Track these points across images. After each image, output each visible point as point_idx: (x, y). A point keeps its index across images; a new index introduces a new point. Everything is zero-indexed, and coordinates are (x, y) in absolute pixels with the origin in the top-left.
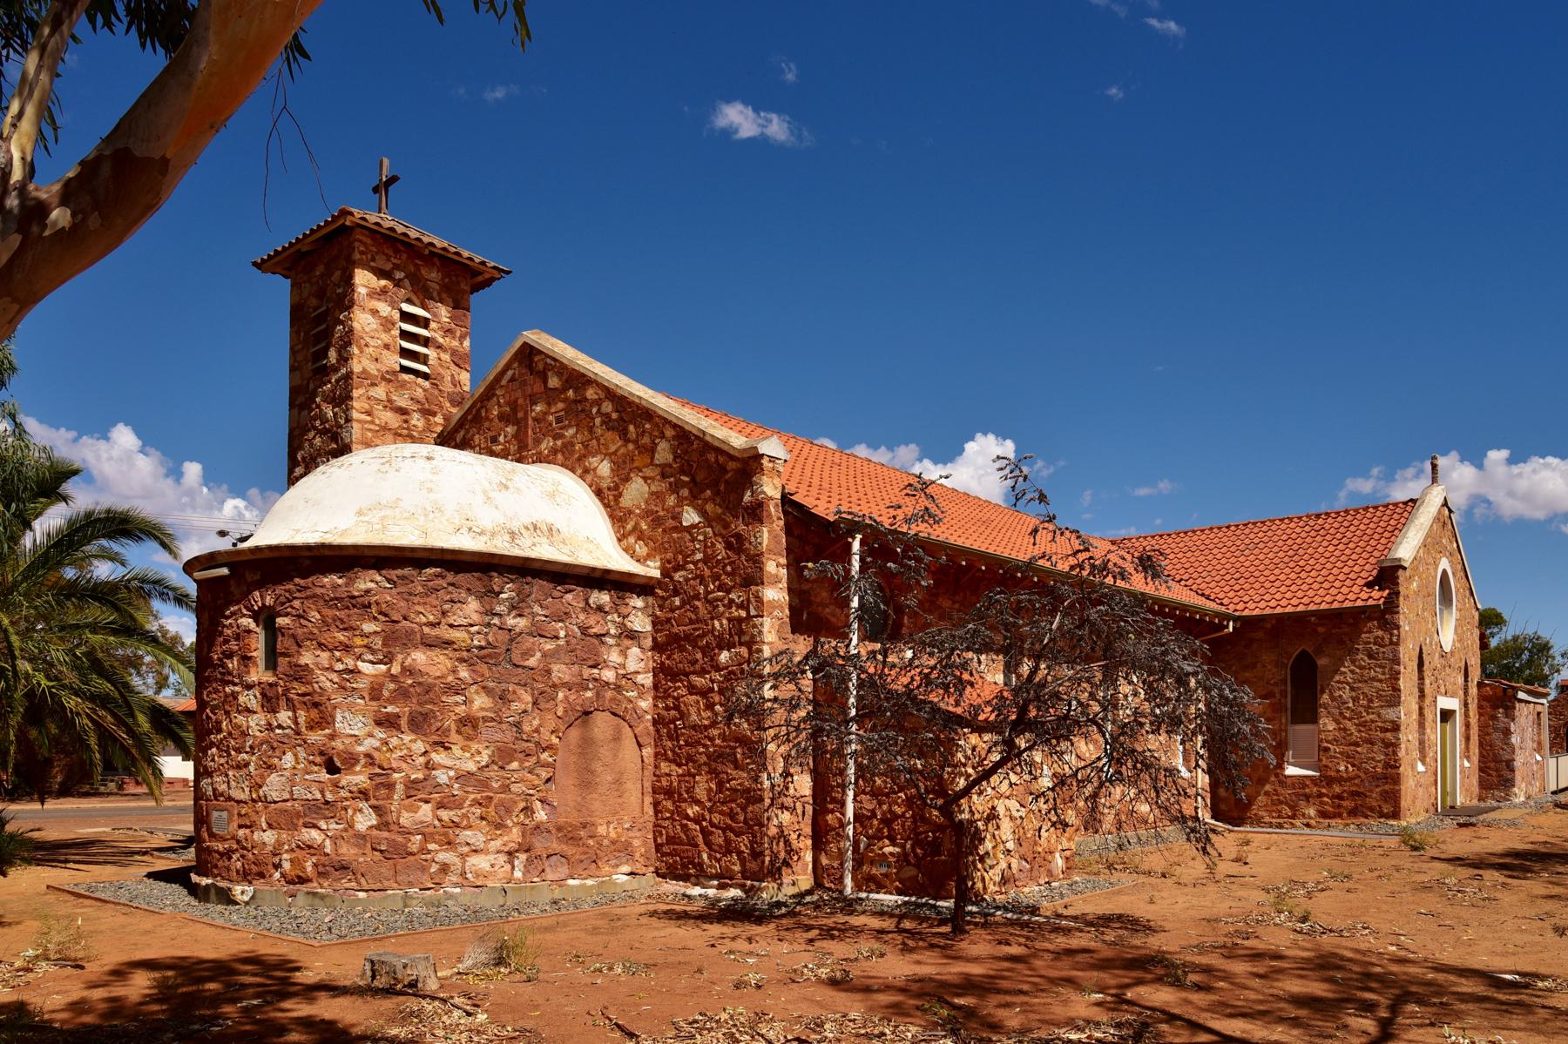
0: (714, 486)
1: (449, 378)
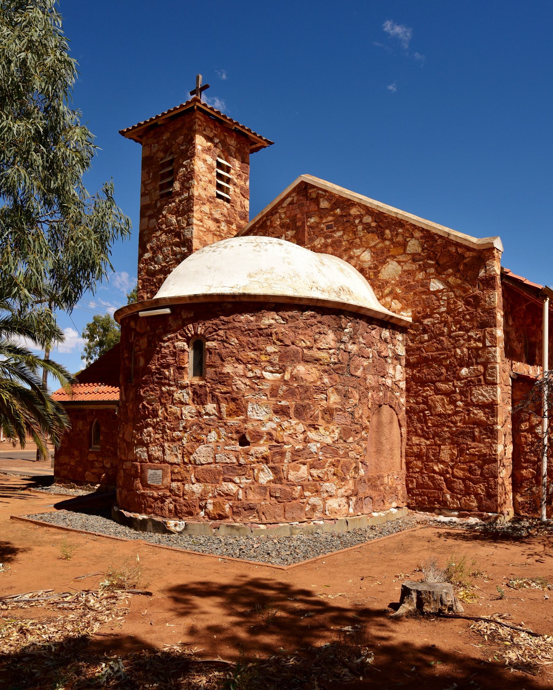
0: (455, 266)
1: (239, 203)
